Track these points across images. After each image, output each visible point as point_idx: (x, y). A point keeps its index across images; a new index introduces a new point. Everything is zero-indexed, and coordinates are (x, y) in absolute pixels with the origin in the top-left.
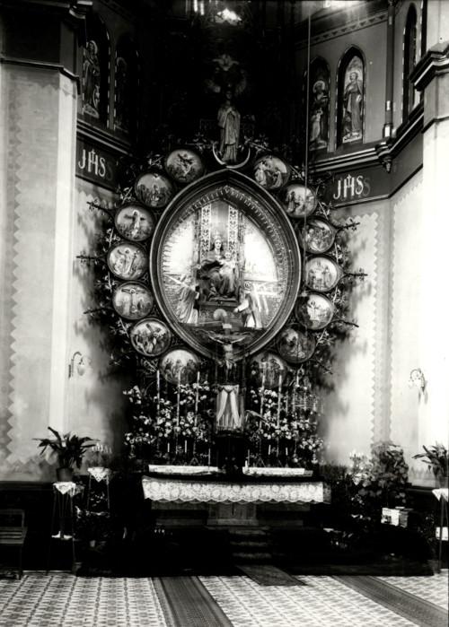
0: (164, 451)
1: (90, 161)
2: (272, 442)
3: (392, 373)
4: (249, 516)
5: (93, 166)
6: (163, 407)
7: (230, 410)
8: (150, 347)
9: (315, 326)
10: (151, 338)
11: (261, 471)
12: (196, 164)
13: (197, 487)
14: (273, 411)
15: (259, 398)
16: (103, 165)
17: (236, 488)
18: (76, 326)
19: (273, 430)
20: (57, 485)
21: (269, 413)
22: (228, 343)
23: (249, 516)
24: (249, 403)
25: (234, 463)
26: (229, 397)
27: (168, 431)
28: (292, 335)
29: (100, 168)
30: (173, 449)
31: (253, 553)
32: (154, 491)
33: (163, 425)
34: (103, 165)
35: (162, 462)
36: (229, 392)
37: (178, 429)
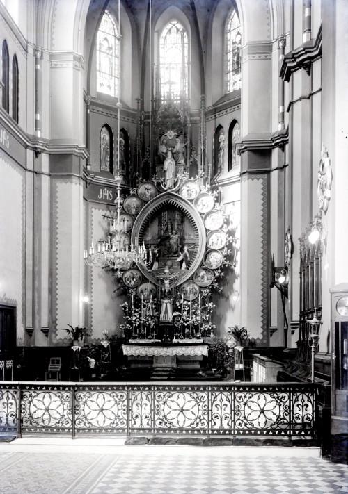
0: (136, 332)
1: (104, 194)
2: (188, 327)
3: (21, 227)
4: (172, 362)
5: (106, 196)
6: (135, 312)
7: (167, 312)
8: (132, 283)
9: (214, 267)
10: (133, 278)
11: (181, 341)
12: (153, 191)
13: (147, 349)
14: (188, 311)
15: (180, 305)
16: (111, 195)
17: (165, 349)
18: (99, 275)
19: (188, 321)
20: (72, 348)
21: (185, 313)
22: (167, 279)
23: (172, 362)
24: (176, 309)
25: (167, 338)
26: (167, 304)
27: (138, 323)
28: (203, 273)
29: (109, 196)
30: (140, 331)
31: (141, 364)
32: (127, 350)
33: (135, 320)
34: (111, 195)
35: (135, 338)
36: (166, 304)
37: (142, 322)
